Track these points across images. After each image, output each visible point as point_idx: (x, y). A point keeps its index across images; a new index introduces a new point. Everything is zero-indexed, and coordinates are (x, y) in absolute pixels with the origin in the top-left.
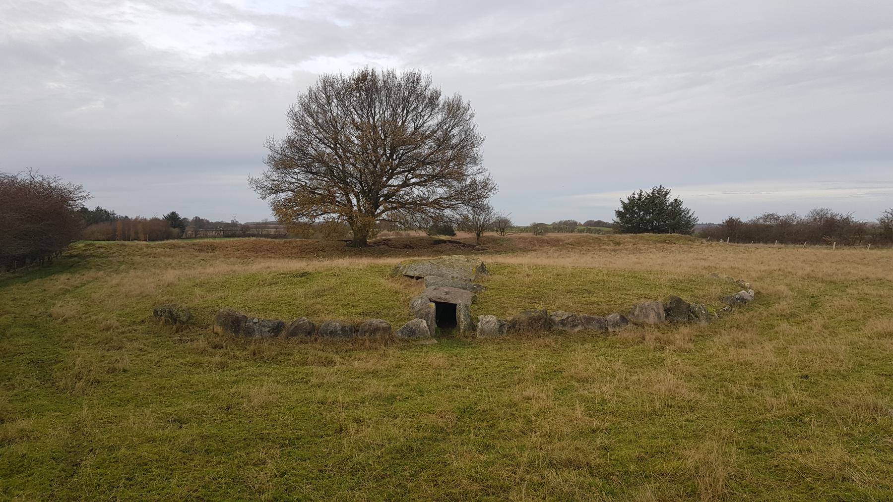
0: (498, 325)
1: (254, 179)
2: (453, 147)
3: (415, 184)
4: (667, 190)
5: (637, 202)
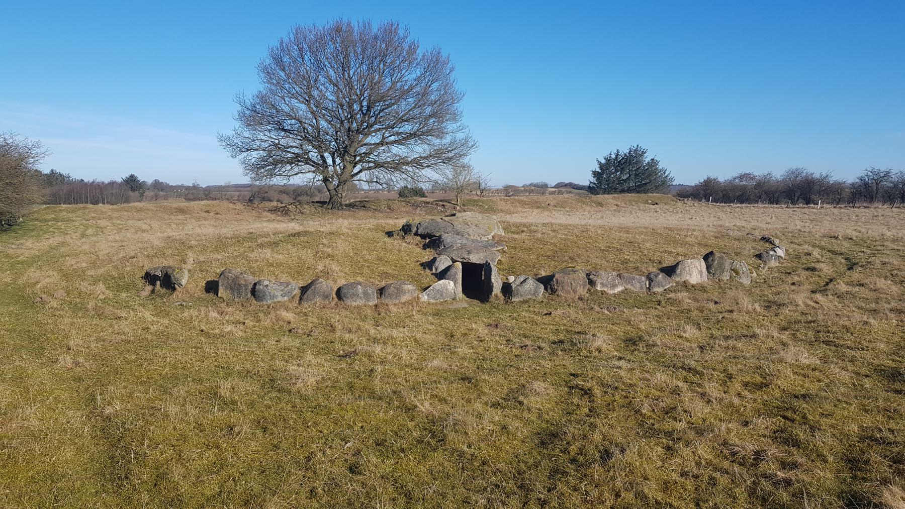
0: (533, 285)
1: (224, 136)
2: (432, 104)
3: (395, 142)
4: (644, 149)
5: (614, 162)
